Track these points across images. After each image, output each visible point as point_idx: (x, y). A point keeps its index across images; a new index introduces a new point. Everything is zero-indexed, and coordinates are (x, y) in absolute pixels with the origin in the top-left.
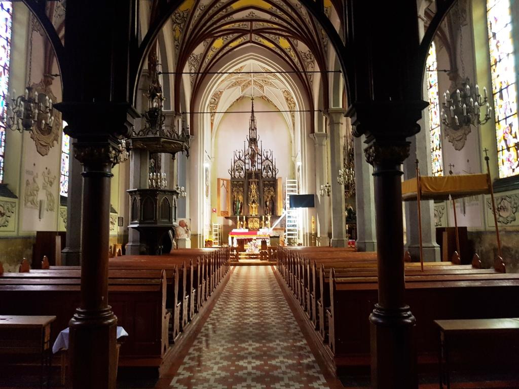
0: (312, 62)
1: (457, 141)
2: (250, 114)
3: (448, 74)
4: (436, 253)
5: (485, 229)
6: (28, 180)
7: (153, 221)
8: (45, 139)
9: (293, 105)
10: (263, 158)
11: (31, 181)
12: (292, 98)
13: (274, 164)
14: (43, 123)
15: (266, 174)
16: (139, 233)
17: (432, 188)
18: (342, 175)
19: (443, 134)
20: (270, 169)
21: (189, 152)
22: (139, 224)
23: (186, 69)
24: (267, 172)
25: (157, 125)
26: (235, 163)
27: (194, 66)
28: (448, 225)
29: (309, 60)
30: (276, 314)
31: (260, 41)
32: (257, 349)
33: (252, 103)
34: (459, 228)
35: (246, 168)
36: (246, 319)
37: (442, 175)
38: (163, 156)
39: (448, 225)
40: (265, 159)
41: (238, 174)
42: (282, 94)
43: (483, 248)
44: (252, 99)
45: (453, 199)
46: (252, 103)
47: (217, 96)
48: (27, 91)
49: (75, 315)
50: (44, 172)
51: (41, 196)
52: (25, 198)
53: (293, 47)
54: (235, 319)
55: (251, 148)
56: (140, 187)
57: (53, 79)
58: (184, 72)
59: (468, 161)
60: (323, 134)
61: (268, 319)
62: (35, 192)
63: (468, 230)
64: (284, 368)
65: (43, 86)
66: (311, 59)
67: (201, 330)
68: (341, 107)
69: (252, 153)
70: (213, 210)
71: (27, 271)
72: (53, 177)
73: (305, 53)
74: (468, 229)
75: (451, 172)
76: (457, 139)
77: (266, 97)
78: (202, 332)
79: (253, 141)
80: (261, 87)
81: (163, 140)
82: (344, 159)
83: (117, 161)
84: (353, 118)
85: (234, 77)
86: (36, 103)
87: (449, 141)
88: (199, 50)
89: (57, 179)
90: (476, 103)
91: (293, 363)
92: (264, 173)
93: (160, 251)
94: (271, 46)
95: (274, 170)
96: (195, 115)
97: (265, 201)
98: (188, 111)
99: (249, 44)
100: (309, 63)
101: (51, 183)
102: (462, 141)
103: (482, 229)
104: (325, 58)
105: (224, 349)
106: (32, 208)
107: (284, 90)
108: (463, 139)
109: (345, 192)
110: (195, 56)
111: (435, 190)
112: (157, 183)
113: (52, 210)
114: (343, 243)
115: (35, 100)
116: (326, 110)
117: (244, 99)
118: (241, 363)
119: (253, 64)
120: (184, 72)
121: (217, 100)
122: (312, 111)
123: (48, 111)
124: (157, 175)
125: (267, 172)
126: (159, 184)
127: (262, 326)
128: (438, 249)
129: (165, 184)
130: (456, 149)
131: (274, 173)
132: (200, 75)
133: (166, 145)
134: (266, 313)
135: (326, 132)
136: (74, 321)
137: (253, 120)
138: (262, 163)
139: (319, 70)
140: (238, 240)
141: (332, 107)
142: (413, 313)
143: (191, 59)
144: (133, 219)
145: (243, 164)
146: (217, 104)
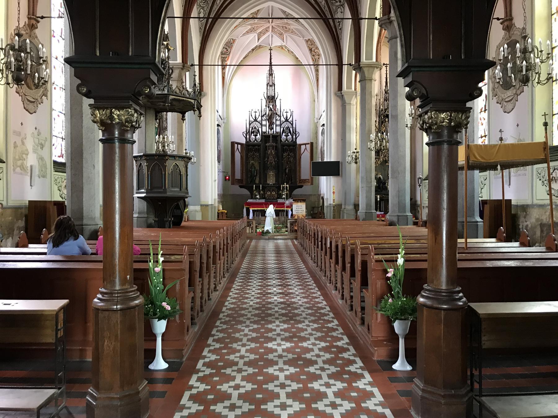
0: (342, 5)
1: (506, 102)
2: (268, 67)
3: (501, 23)
4: (479, 228)
5: (532, 202)
6: (15, 142)
7: (162, 190)
8: (33, 94)
9: (317, 57)
10: (283, 119)
11: (19, 143)
12: (317, 48)
13: (294, 126)
14: (36, 77)
17: (482, 158)
19: (491, 93)
20: (290, 132)
21: (202, 112)
22: (146, 193)
23: (194, 13)
24: (287, 136)
25: (164, 79)
26: (250, 124)
27: (203, 8)
28: (490, 197)
29: (338, 4)
30: (302, 293)
33: (271, 52)
34: (506, 200)
36: (270, 298)
37: (487, 143)
38: (171, 117)
39: (490, 197)
40: (284, 120)
42: (304, 43)
43: (528, 223)
44: (271, 50)
45: (502, 169)
46: (271, 52)
47: (229, 45)
48: (17, 38)
49: (98, 296)
50: (33, 133)
51: (32, 160)
52: (13, 163)
55: (269, 107)
57: (38, 22)
58: (192, 16)
59: (518, 125)
60: (352, 92)
61: (293, 298)
62: (24, 156)
63: (513, 203)
64: (316, 351)
65: (27, 30)
67: (222, 309)
68: (374, 60)
69: (270, 114)
70: (225, 177)
71: (26, 246)
72: (44, 139)
74: (512, 202)
75: (501, 139)
76: (506, 100)
77: (286, 47)
78: (224, 312)
79: (271, 99)
81: (171, 97)
86: (28, 53)
87: (498, 103)
89: (49, 140)
90: (538, 60)
91: (326, 345)
92: (284, 137)
95: (295, 133)
96: (204, 67)
97: (284, 168)
98: (196, 62)
100: (338, 7)
101: (42, 146)
102: (512, 102)
103: (529, 202)
105: (243, 331)
106: (21, 174)
108: (514, 99)
109: (376, 159)
111: (485, 159)
112: (164, 146)
113: (44, 176)
115: (26, 49)
116: (357, 64)
118: (270, 345)
119: (272, 6)
120: (192, 16)
121: (229, 50)
123: (42, 62)
124: (164, 138)
125: (287, 136)
126: (166, 148)
127: (289, 305)
128: (481, 224)
129: (173, 147)
130: (505, 112)
131: (294, 137)
132: (210, 20)
133: (174, 103)
134: (290, 291)
135: (355, 89)
136: (98, 303)
137: (271, 74)
138: (281, 125)
141: (364, 61)
142: (465, 296)
144: (139, 188)
145: (259, 125)
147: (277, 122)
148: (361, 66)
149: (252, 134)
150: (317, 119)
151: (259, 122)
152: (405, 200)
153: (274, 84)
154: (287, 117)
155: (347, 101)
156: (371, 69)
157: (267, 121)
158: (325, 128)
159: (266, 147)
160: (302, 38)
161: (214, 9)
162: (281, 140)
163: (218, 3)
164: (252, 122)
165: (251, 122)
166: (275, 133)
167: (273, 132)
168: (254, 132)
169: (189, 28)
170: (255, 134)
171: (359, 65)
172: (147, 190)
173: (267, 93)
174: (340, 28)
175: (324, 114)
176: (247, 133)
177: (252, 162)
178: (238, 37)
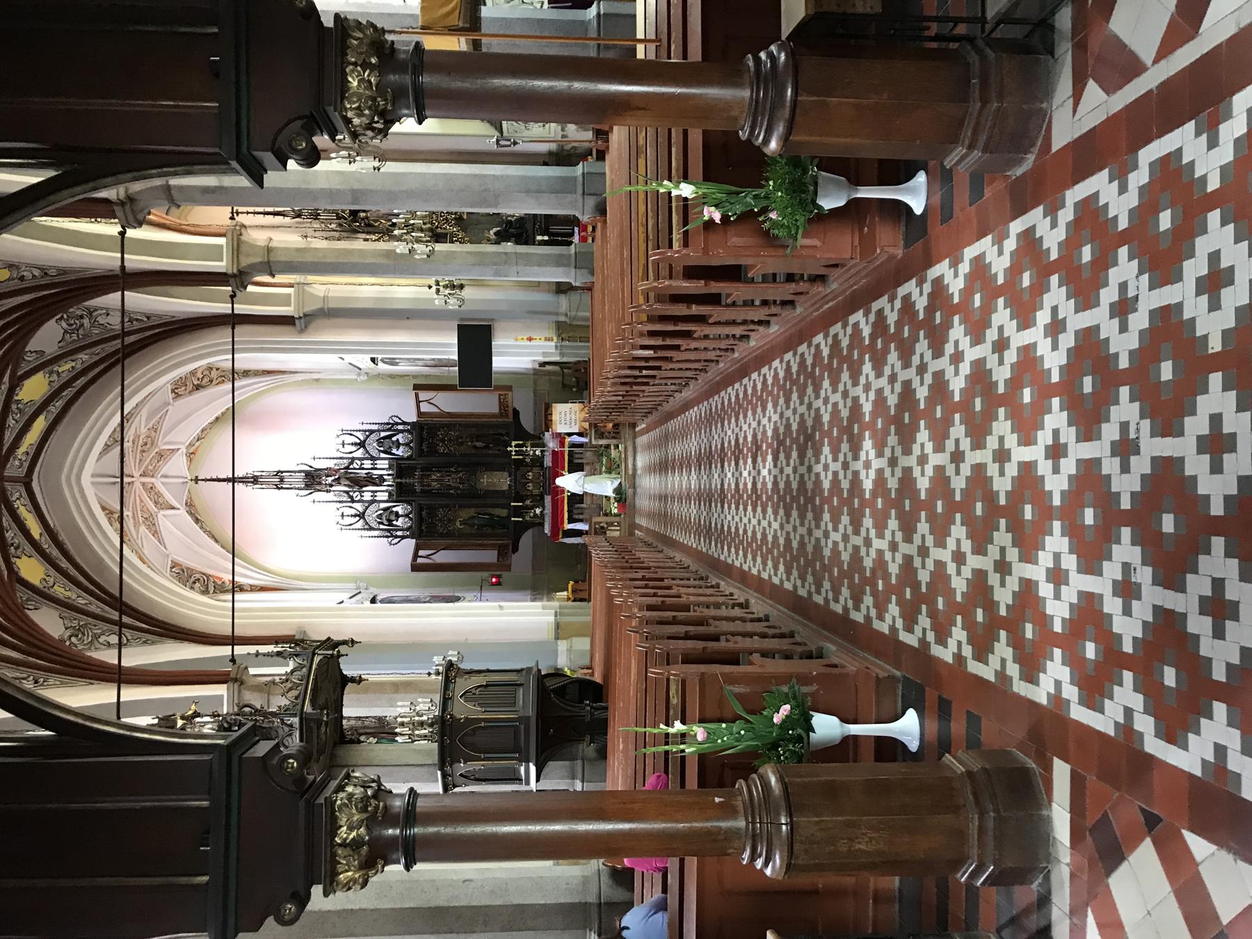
0: (91, 313)
2: (239, 487)
7: (522, 726)
9: (214, 374)
12: (193, 373)
13: (375, 427)
15: (401, 448)
16: (550, 763)
18: (410, 245)
20: (390, 437)
22: (527, 761)
23: (109, 657)
24: (398, 445)
26: (371, 529)
27: (96, 637)
29: (86, 321)
31: (27, 453)
32: (835, 452)
35: (386, 498)
36: (764, 484)
38: (354, 709)
40: (362, 450)
41: (401, 519)
42: (181, 402)
44: (196, 480)
47: (186, 576)
49: (759, 867)
53: (46, 364)
54: (764, 511)
55: (331, 486)
56: (434, 765)
60: (298, 294)
66: (82, 317)
68: (221, 241)
73: (66, 332)
77: (191, 445)
78: (795, 587)
79: (313, 480)
80: (161, 455)
81: (308, 708)
82: (366, 240)
83: (373, 781)
84: (266, 164)
85: (132, 529)
88: (50, 622)
92: (400, 452)
93: (597, 709)
94: (40, 424)
95: (391, 427)
96: (239, 632)
98: (226, 651)
99: (35, 485)
100: (94, 323)
104: (81, 275)
107: (171, 396)
110: (68, 633)
112: (422, 724)
114: (584, 253)
116: (232, 281)
117: (196, 503)
118: (868, 485)
120: (116, 662)
121: (198, 576)
122: (234, 320)
124: (402, 724)
125: (398, 445)
126: (425, 718)
127: (781, 443)
129: (425, 703)
131: (400, 427)
132: (126, 619)
133: (321, 701)
135: (291, 286)
136: (773, 867)
137: (255, 480)
138: (373, 458)
139: (119, 293)
140: (569, 523)
141: (224, 263)
143: (78, 644)
144: (517, 779)
145: (373, 508)
146: (208, 576)
147: (365, 466)
148: (235, 271)
149: (394, 523)
150: (359, 375)
151: (367, 508)
152: (548, 178)
153: (278, 472)
154: (356, 444)
155: (319, 306)
156: (243, 248)
157: (364, 489)
158: (380, 357)
159: (422, 491)
160: (170, 407)
161: (98, 611)
162: (409, 458)
163: (84, 602)
164: (367, 523)
165: (367, 527)
166: (390, 472)
167: (389, 475)
168: (388, 518)
169: (150, 668)
170: (393, 517)
171: (234, 276)
172: (520, 761)
173: (299, 489)
174: (145, 319)
175: (349, 358)
176: (392, 536)
177: (458, 524)
178: (168, 556)
